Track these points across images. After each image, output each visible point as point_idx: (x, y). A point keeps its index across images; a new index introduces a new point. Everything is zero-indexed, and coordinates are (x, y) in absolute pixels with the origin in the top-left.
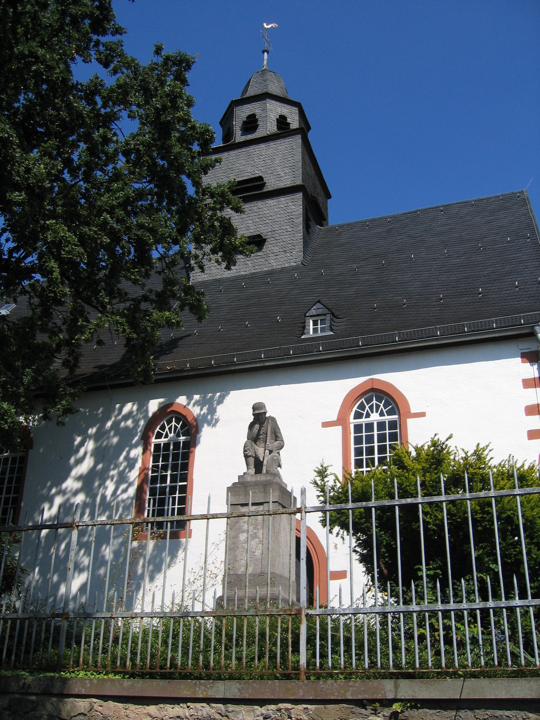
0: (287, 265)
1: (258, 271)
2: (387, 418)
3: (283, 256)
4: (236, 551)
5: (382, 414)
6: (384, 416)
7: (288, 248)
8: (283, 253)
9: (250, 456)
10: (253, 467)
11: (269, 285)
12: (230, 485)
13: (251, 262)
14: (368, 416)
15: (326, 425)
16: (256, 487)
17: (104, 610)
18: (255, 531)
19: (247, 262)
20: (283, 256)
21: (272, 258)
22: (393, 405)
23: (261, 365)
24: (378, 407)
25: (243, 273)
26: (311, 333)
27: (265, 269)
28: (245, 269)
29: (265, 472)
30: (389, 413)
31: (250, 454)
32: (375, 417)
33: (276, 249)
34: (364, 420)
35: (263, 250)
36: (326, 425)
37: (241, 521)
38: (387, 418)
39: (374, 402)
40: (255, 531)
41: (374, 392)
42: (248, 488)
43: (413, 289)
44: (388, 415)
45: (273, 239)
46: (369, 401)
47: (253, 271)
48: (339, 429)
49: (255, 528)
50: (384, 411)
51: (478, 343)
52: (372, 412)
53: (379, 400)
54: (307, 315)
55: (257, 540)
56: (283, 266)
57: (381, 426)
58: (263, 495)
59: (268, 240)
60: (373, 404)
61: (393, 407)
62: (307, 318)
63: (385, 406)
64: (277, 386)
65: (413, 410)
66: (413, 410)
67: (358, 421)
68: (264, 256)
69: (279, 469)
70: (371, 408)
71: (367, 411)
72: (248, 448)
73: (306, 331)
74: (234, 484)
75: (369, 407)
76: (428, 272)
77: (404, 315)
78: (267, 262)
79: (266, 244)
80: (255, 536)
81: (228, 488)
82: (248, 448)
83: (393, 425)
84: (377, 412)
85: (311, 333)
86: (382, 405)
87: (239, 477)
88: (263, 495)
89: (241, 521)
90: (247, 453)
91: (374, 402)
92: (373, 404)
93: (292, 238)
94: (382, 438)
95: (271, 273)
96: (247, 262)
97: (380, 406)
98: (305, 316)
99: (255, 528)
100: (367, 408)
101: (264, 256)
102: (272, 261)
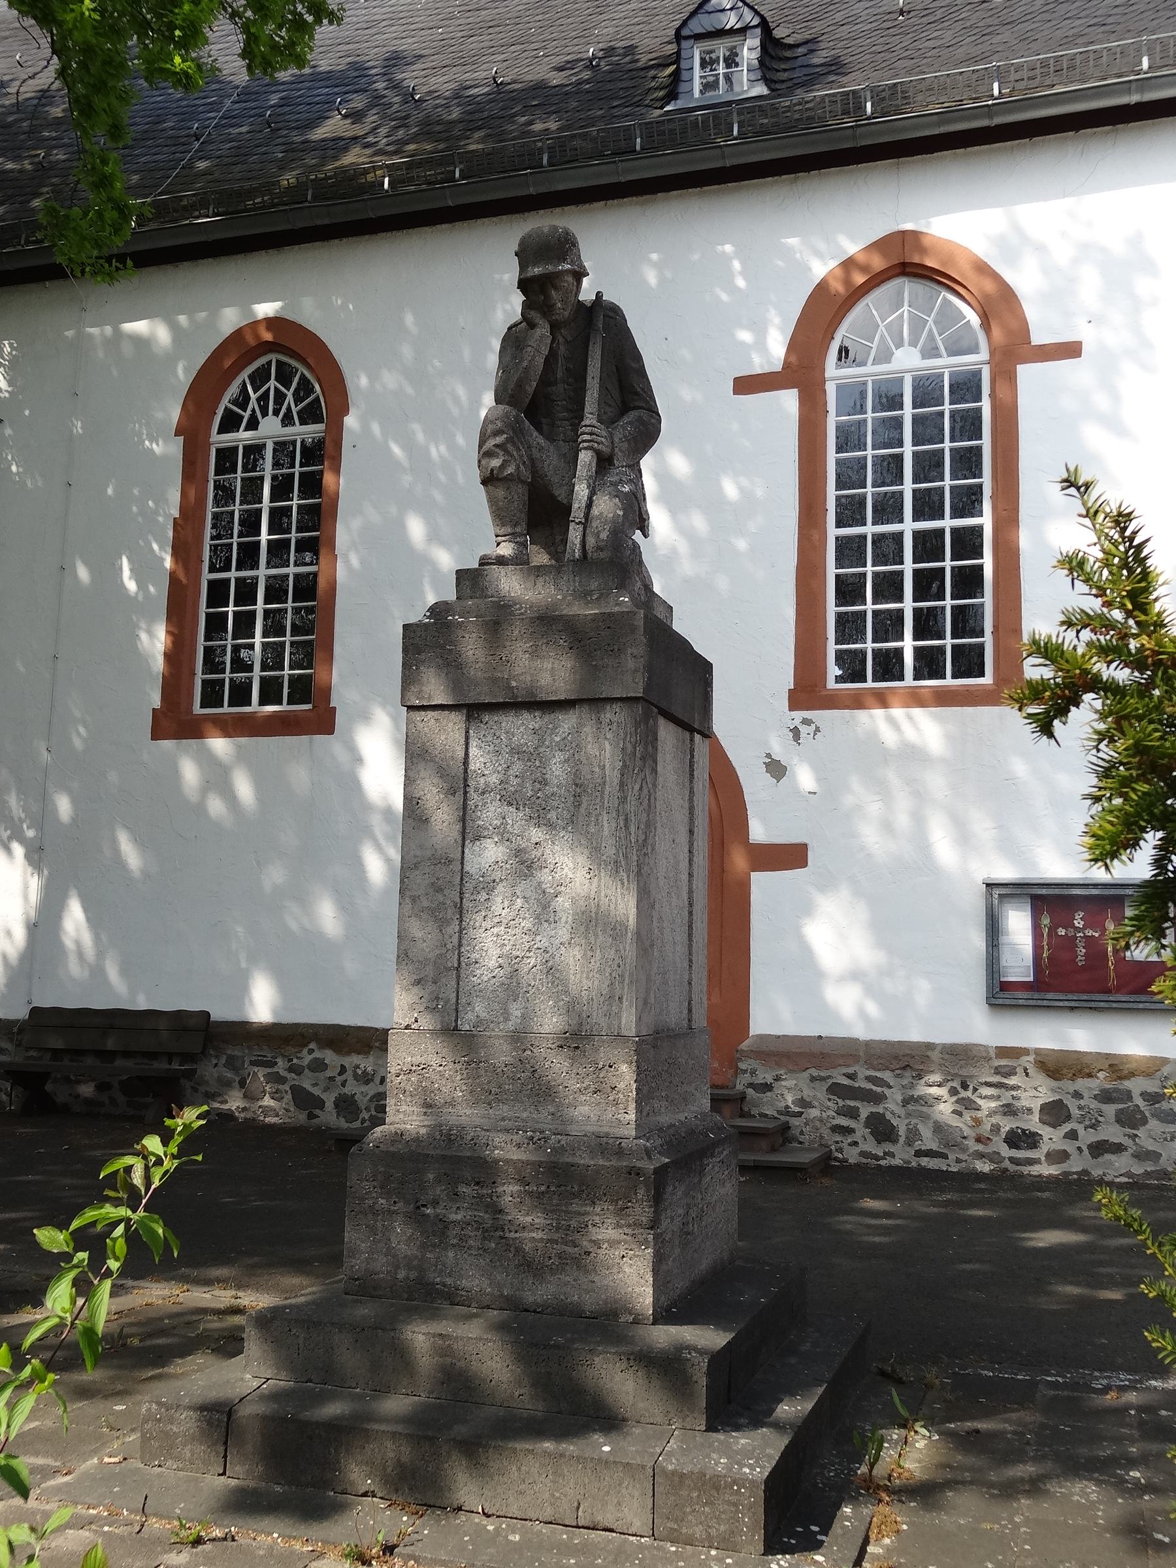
5: (287, 420)
12: (417, 615)
14: (253, 425)
15: (746, 385)
17: (742, 1156)
24: (280, 397)
26: (697, 94)
32: (271, 428)
34: (243, 436)
36: (746, 385)
48: (789, 400)
50: (294, 410)
51: (1113, 123)
52: (265, 414)
57: (283, 449)
65: (1039, 337)
66: (1039, 337)
67: (228, 439)
69: (638, 536)
73: (683, 87)
83: (315, 453)
84: (276, 413)
85: (697, 94)
91: (272, 383)
97: (286, 396)
100: (253, 403)
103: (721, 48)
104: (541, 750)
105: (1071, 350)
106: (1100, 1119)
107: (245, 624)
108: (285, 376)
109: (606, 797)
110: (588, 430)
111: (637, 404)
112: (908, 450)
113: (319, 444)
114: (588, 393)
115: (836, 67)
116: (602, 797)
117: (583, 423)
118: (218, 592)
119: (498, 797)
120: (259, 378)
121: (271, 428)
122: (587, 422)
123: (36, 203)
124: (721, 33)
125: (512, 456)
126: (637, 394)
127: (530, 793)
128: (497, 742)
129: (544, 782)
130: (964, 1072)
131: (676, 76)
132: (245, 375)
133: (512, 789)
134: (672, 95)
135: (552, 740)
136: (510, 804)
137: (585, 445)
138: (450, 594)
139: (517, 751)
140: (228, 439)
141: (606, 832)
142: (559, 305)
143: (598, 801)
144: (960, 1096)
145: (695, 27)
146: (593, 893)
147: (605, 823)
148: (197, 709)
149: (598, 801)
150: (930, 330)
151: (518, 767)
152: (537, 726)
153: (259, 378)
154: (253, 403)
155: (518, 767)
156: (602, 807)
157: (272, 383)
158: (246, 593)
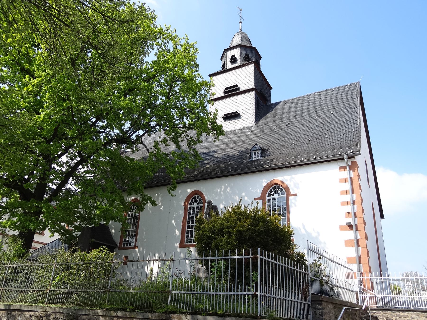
24: (197, 201)
57: (197, 207)
103: (256, 152)
105: (295, 195)
106: (88, 275)
107: (192, 232)
108: (198, 197)
113: (202, 207)
115: (270, 154)
118: (188, 227)
120: (195, 198)
121: (196, 205)
123: (138, 185)
124: (256, 150)
131: (250, 155)
132: (193, 198)
134: (250, 158)
140: (269, 198)
145: (254, 149)
148: (185, 244)
153: (195, 198)
154: (273, 192)
157: (276, 189)
158: (192, 227)
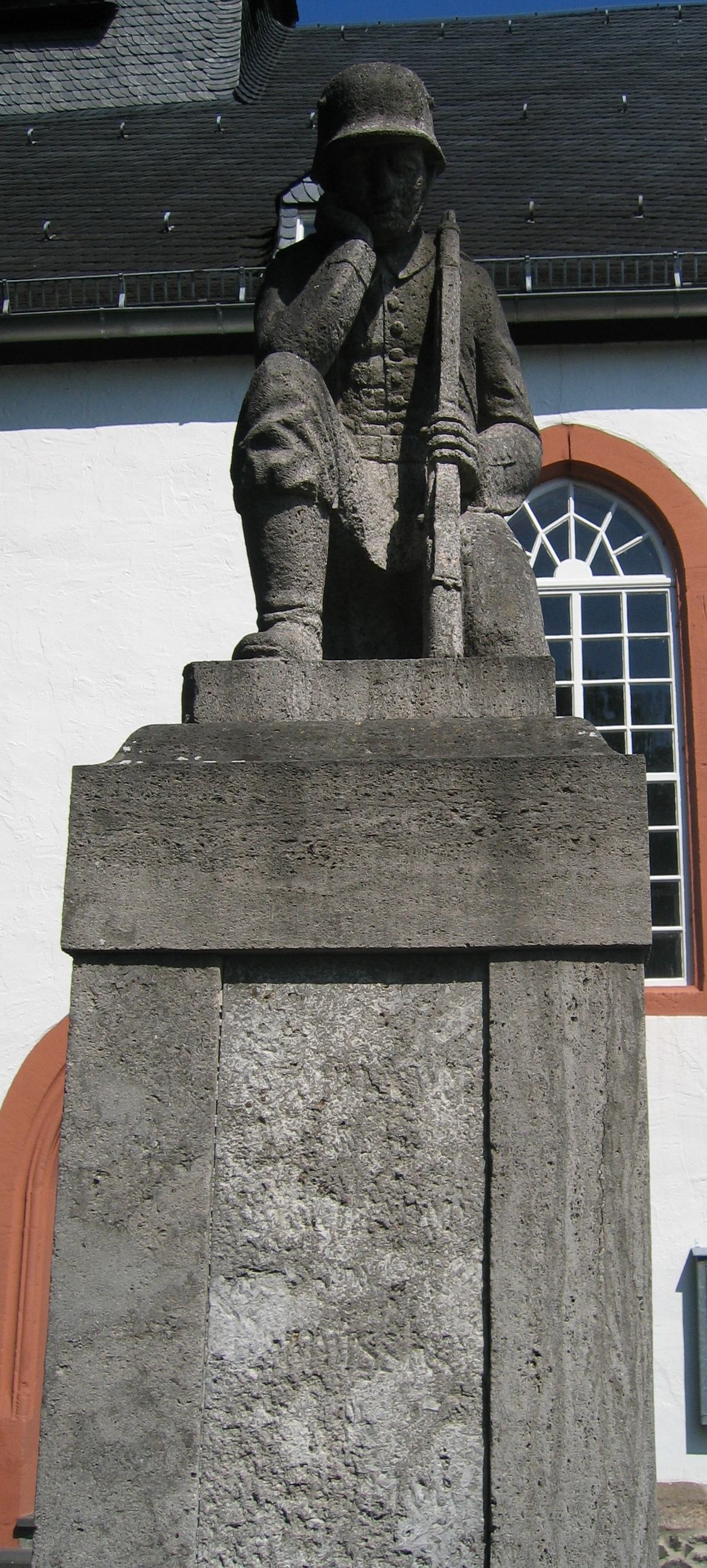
0: (183, 97)
1: (82, 105)
2: (622, 581)
3: (169, 66)
4: (172, 1481)
5: (601, 566)
6: (612, 572)
7: (189, 45)
8: (172, 57)
9: (306, 494)
10: (315, 599)
11: (122, 141)
12: (103, 749)
13: (61, 75)
16: (401, 782)
18: (393, 1265)
19: (46, 76)
20: (169, 66)
21: (131, 68)
22: (650, 533)
23: (116, 331)
24: (585, 537)
25: (30, 109)
27: (107, 103)
28: (37, 98)
29: (458, 647)
30: (633, 564)
31: (306, 474)
33: (147, 44)
35: (104, 42)
37: (225, 1144)
38: (622, 581)
39: (571, 515)
40: (393, 1265)
41: (570, 477)
42: (315, 792)
43: (652, 178)
44: (627, 572)
45: (141, 11)
46: (549, 511)
47: (64, 106)
49: (394, 1230)
50: (613, 554)
52: (564, 555)
53: (592, 510)
54: (288, 198)
55: (416, 1369)
56: (172, 98)
57: (600, 610)
58: (476, 867)
59: (122, 12)
60: (566, 525)
61: (647, 543)
62: (283, 212)
63: (616, 536)
64: (174, 426)
68: (105, 62)
70: (559, 538)
71: (543, 548)
72: (295, 412)
74: (147, 741)
75: (549, 536)
76: (690, 143)
77: (649, 241)
78: (114, 82)
79: (115, 23)
80: (387, 1324)
81: (81, 773)
82: (295, 412)
84: (582, 555)
86: (602, 530)
87: (193, 678)
88: (476, 867)
89: (225, 1144)
90: (278, 457)
91: (571, 515)
92: (566, 525)
93: (204, 15)
94: (601, 659)
95: (131, 114)
96: (46, 76)
97: (596, 533)
98: (279, 204)
99: (394, 1230)
101: (105, 62)
102: (133, 80)
104: (403, 1063)
109: (570, 1178)
110: (448, 426)
111: (508, 412)
112: (578, 683)
114: (445, 366)
116: (560, 1175)
117: (440, 414)
119: (296, 1173)
122: (446, 413)
125: (311, 447)
126: (508, 395)
127: (376, 1165)
128: (294, 1041)
129: (411, 1141)
130: (675, 1524)
133: (332, 1154)
135: (429, 1041)
136: (326, 1190)
137: (446, 452)
138: (169, 711)
139: (340, 1065)
141: (573, 1262)
142: (397, 202)
143: (550, 1185)
144: (670, 1559)
146: (544, 1412)
147: (570, 1240)
149: (550, 1185)
150: (602, 544)
151: (345, 1102)
152: (391, 1007)
155: (345, 1102)
156: (561, 1200)
